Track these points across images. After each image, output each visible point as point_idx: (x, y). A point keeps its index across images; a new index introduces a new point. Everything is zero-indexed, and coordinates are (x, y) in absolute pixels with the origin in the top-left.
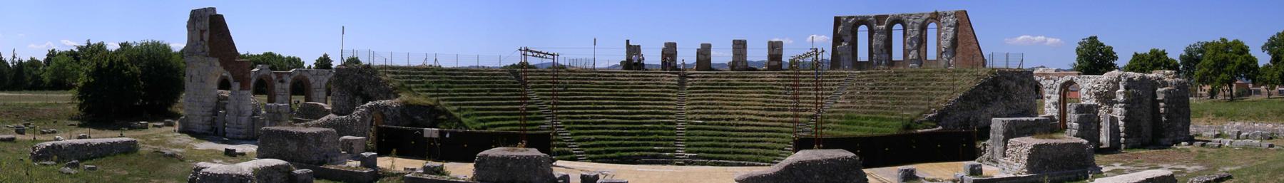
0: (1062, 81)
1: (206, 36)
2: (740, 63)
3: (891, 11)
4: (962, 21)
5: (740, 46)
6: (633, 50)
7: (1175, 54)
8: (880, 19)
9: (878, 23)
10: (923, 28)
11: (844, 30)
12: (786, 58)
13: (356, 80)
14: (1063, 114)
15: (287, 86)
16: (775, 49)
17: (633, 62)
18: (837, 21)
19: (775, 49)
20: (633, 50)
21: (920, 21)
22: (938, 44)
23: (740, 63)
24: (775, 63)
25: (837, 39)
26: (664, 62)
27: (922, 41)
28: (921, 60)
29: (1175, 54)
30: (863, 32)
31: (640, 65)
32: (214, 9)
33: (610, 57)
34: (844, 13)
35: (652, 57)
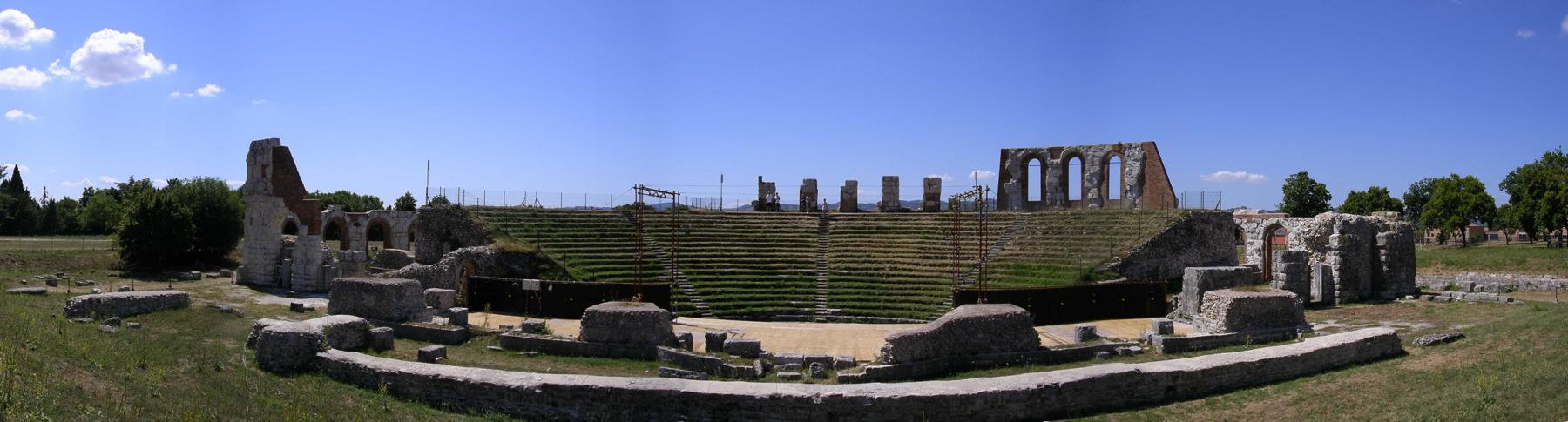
0: (1266, 224)
1: (269, 171)
2: (890, 203)
3: (1067, 143)
4: (1150, 154)
5: (891, 184)
6: (766, 188)
7: (1398, 192)
8: (1054, 152)
9: (1052, 157)
10: (1105, 162)
11: (1013, 165)
12: (945, 197)
13: (443, 224)
14: (1268, 263)
15: (364, 230)
16: (932, 186)
17: (767, 202)
18: (1005, 154)
19: (932, 186)
20: (766, 188)
21: (1101, 154)
22: (1123, 180)
23: (890, 203)
24: (932, 203)
25: (1004, 175)
26: (803, 202)
27: (1103, 178)
28: (1102, 199)
29: (1398, 192)
30: (1034, 167)
31: (774, 206)
32: (278, 140)
33: (739, 196)
34: (1012, 145)
35: (789, 196)
